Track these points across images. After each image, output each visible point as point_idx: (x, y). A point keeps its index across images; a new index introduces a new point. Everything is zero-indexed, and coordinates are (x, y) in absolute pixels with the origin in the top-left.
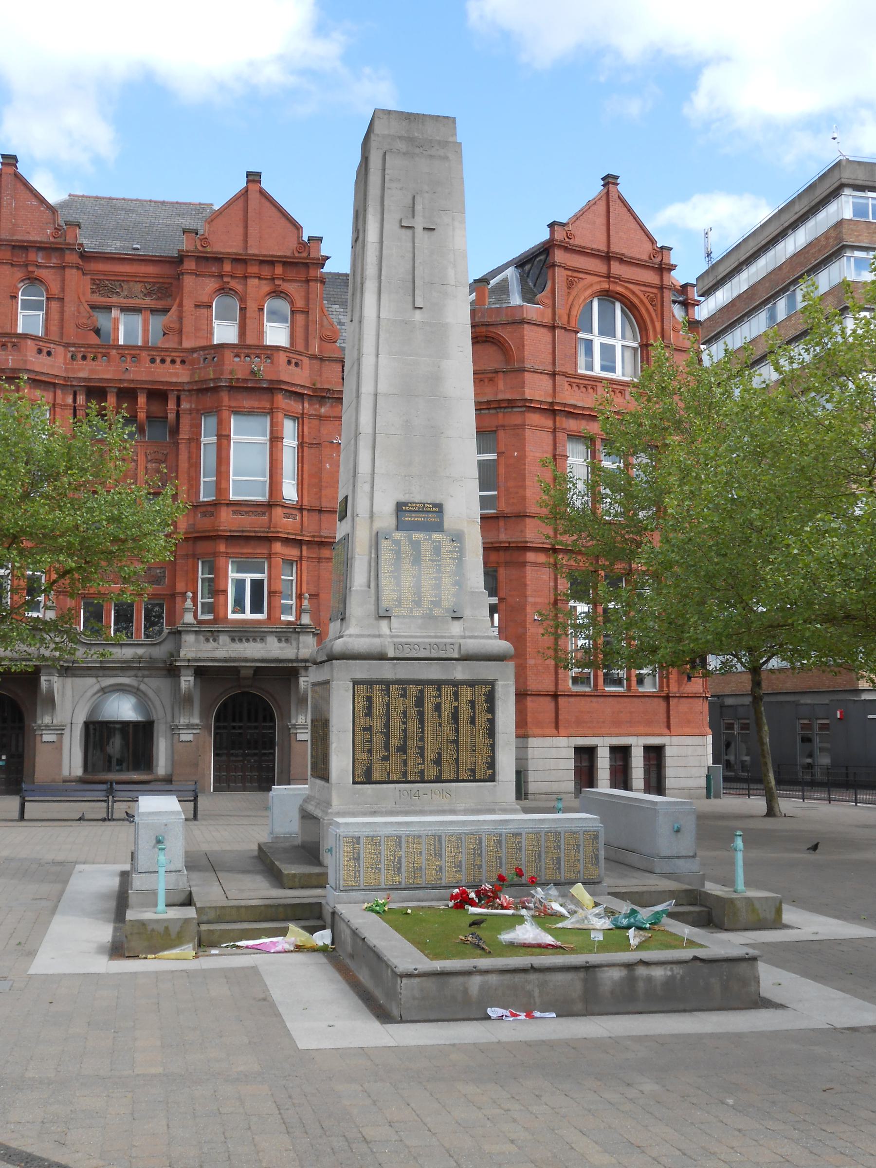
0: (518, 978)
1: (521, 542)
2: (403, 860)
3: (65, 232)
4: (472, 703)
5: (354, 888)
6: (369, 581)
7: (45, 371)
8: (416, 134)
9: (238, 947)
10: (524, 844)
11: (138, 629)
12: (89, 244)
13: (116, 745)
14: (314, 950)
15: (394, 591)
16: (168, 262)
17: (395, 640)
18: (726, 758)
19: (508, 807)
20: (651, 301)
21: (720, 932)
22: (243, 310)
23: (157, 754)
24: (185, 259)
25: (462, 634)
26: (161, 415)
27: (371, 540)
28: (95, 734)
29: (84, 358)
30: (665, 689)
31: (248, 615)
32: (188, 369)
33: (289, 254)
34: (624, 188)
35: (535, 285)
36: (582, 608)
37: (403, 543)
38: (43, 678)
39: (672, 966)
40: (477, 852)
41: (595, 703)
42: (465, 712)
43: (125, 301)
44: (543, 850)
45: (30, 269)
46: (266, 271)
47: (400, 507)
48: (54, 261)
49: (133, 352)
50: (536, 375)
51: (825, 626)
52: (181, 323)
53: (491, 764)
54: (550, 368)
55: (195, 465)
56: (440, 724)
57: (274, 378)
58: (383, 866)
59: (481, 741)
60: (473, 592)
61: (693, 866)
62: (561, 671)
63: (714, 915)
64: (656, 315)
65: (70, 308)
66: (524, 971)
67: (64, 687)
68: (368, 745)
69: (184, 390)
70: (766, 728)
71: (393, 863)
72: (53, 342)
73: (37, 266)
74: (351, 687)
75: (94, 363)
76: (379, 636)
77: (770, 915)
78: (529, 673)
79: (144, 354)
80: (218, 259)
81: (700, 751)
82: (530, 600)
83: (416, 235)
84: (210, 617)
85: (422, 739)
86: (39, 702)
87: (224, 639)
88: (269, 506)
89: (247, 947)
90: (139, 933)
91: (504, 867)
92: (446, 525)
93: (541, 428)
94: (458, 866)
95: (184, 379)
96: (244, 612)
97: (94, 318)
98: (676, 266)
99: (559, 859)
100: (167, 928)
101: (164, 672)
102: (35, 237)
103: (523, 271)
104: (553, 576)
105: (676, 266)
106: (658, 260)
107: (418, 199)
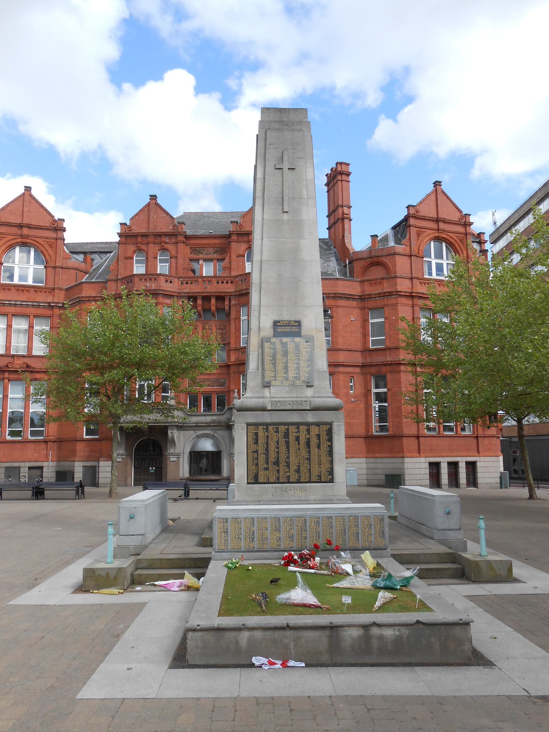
0: (278, 634)
2: (255, 533)
4: (318, 436)
6: (258, 366)
8: (284, 119)
9: (155, 585)
12: (189, 232)
13: (204, 463)
15: (272, 371)
16: (225, 237)
17: (272, 399)
18: (514, 468)
19: (342, 498)
20: (461, 241)
21: (468, 584)
23: (223, 468)
25: (313, 395)
26: (222, 307)
27: (259, 343)
28: (194, 457)
29: (187, 283)
30: (476, 433)
34: (444, 187)
37: (277, 344)
38: (169, 431)
39: (400, 627)
40: (303, 528)
41: (439, 440)
42: (314, 441)
44: (347, 527)
47: (276, 324)
48: (173, 240)
49: (209, 279)
52: (231, 265)
53: (331, 472)
54: (410, 276)
56: (299, 449)
58: (243, 537)
59: (325, 459)
64: (464, 247)
65: (180, 261)
66: (282, 628)
70: (527, 452)
71: (249, 535)
74: (246, 426)
76: (263, 397)
77: (504, 573)
78: (404, 425)
79: (214, 280)
81: (495, 464)
85: (288, 457)
86: (168, 443)
89: (160, 586)
91: (321, 538)
92: (303, 333)
93: (406, 305)
94: (291, 537)
95: (232, 290)
98: (473, 223)
99: (357, 533)
100: (108, 573)
101: (226, 428)
105: (473, 223)
106: (464, 220)
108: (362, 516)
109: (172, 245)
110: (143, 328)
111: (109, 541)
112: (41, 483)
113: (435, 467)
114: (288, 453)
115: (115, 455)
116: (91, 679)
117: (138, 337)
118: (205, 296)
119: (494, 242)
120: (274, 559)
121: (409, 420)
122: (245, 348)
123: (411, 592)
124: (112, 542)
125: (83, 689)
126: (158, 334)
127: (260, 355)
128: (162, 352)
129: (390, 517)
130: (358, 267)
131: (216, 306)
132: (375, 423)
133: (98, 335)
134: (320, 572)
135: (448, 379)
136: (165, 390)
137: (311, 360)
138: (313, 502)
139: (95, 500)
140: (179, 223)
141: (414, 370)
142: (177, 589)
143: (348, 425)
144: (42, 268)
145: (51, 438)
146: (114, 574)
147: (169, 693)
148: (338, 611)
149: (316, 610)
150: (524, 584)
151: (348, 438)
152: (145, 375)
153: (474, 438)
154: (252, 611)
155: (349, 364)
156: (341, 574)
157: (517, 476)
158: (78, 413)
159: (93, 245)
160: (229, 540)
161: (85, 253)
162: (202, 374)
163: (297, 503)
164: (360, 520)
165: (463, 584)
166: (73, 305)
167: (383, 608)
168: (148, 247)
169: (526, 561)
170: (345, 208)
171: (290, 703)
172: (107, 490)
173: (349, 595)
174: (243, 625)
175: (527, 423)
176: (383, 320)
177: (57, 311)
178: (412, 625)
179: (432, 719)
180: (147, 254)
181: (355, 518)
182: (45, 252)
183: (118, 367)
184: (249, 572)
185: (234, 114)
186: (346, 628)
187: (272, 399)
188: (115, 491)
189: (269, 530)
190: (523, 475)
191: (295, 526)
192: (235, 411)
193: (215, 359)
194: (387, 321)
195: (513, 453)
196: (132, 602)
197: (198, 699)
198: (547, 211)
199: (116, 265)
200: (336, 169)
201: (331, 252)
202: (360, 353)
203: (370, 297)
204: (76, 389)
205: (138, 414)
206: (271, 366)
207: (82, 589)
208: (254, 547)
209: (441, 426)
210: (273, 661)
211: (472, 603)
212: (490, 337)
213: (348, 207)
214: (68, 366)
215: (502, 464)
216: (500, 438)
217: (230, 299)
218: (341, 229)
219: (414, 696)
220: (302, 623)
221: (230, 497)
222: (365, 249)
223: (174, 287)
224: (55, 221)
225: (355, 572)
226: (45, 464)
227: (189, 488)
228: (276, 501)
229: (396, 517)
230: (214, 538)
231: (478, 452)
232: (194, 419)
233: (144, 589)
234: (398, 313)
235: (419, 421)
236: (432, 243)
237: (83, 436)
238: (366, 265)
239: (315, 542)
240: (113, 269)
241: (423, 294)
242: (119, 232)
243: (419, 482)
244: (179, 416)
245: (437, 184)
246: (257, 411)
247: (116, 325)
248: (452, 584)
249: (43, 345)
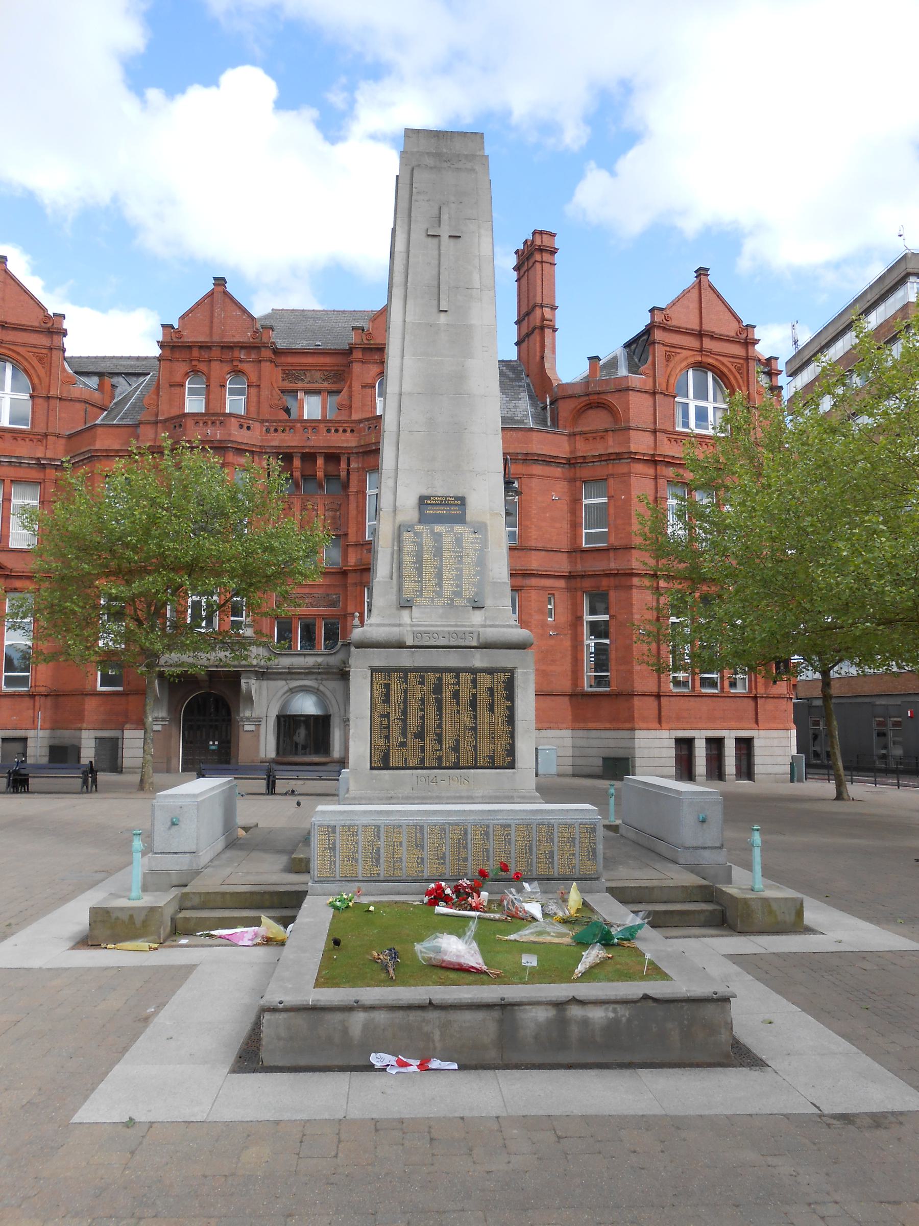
0: (413, 1016)
1: (629, 569)
2: (382, 851)
3: (262, 334)
5: (329, 879)
7: (245, 442)
8: (445, 150)
9: (211, 936)
12: (281, 344)
13: (301, 735)
15: (415, 582)
17: (414, 629)
18: (815, 749)
19: (527, 794)
20: (739, 370)
21: (732, 936)
23: (333, 741)
24: (354, 351)
25: (483, 623)
26: (336, 473)
28: (285, 725)
29: (276, 430)
32: (357, 437)
35: (639, 361)
37: (424, 535)
39: (616, 1006)
40: (461, 844)
41: (693, 702)
42: (483, 699)
43: (308, 385)
44: (534, 843)
45: (235, 363)
47: (423, 501)
48: (253, 356)
53: (511, 751)
54: (651, 426)
56: (458, 712)
58: (360, 857)
59: (501, 728)
60: (495, 582)
63: (728, 914)
64: (743, 381)
65: (265, 393)
66: (421, 1007)
68: (385, 731)
70: (835, 723)
72: (252, 419)
75: (284, 434)
76: (400, 625)
77: (790, 918)
79: (322, 425)
83: (442, 243)
85: (440, 726)
86: (241, 701)
89: (220, 937)
90: (103, 922)
91: (491, 861)
92: (468, 518)
93: (644, 476)
94: (442, 858)
95: (353, 444)
97: (284, 400)
98: (759, 340)
99: (552, 853)
100: (131, 917)
101: (339, 676)
102: (238, 339)
103: (630, 350)
105: (759, 340)
106: (744, 336)
107: (445, 210)
109: (252, 364)
110: (199, 505)
111: (135, 863)
112: (23, 765)
113: (685, 746)
114: (439, 719)
115: (150, 719)
116: (96, 1091)
117: (190, 519)
119: (793, 374)
120: (413, 894)
121: (644, 667)
122: (370, 543)
123: (636, 949)
124: (139, 866)
125: (84, 1107)
126: (226, 516)
127: (395, 553)
128: (232, 548)
129: (608, 827)
130: (566, 409)
131: (325, 471)
132: (588, 674)
133: (121, 515)
134: (487, 915)
135: (711, 601)
136: (236, 612)
137: (481, 563)
138: (480, 800)
139: (114, 795)
140: (263, 327)
141: (655, 585)
142: (250, 943)
143: (542, 674)
144: (26, 398)
145: (42, 690)
146: (142, 917)
147: (228, 1114)
148: (515, 979)
149: (477, 977)
150: (822, 936)
151: (540, 697)
152: (201, 586)
153: (750, 699)
154: (372, 979)
155: (547, 573)
157: (818, 762)
158: (87, 648)
159: (114, 361)
160: (338, 861)
161: (100, 375)
162: (300, 585)
163: (454, 801)
164: (556, 830)
165: (722, 936)
166: (80, 464)
167: (589, 975)
168: (210, 366)
169: (827, 898)
170: (547, 309)
171: (430, 1127)
172: (137, 778)
173: (535, 953)
174: (357, 1002)
175: (837, 676)
176: (605, 500)
177: (52, 474)
179: (662, 1152)
180: (208, 379)
181: (549, 827)
182: (32, 371)
183: (157, 570)
184: (370, 915)
185: (340, 147)
186: (527, 1007)
187: (414, 629)
188: (150, 781)
190: (828, 760)
191: (448, 838)
192: (353, 649)
193: (321, 560)
195: (813, 726)
196: (171, 964)
197: (278, 1122)
198: (882, 324)
199: (155, 397)
200: (533, 241)
201: (520, 384)
202: (565, 555)
203: (584, 460)
204: (83, 608)
205: (189, 650)
207: (87, 941)
209: (697, 678)
210: (405, 1060)
211: (735, 966)
212: (781, 532)
213: (552, 308)
214: (70, 567)
215: (794, 741)
216: (793, 701)
217: (349, 460)
218: (538, 344)
219: (634, 1116)
220: (455, 999)
221: (342, 792)
222: (578, 380)
223: (253, 437)
224: (49, 317)
225: (545, 915)
226: (31, 734)
227: (274, 777)
228: (418, 798)
229: (617, 826)
230: (312, 859)
231: (757, 722)
232: (286, 662)
233: (193, 943)
234: (630, 490)
235: (660, 670)
237: (96, 686)
238: (579, 407)
239: (481, 867)
240: (150, 404)
241: (673, 457)
243: (659, 771)
244: (259, 655)
245: (702, 272)
246: (388, 648)
247: (152, 499)
248: (704, 936)
249: (25, 532)
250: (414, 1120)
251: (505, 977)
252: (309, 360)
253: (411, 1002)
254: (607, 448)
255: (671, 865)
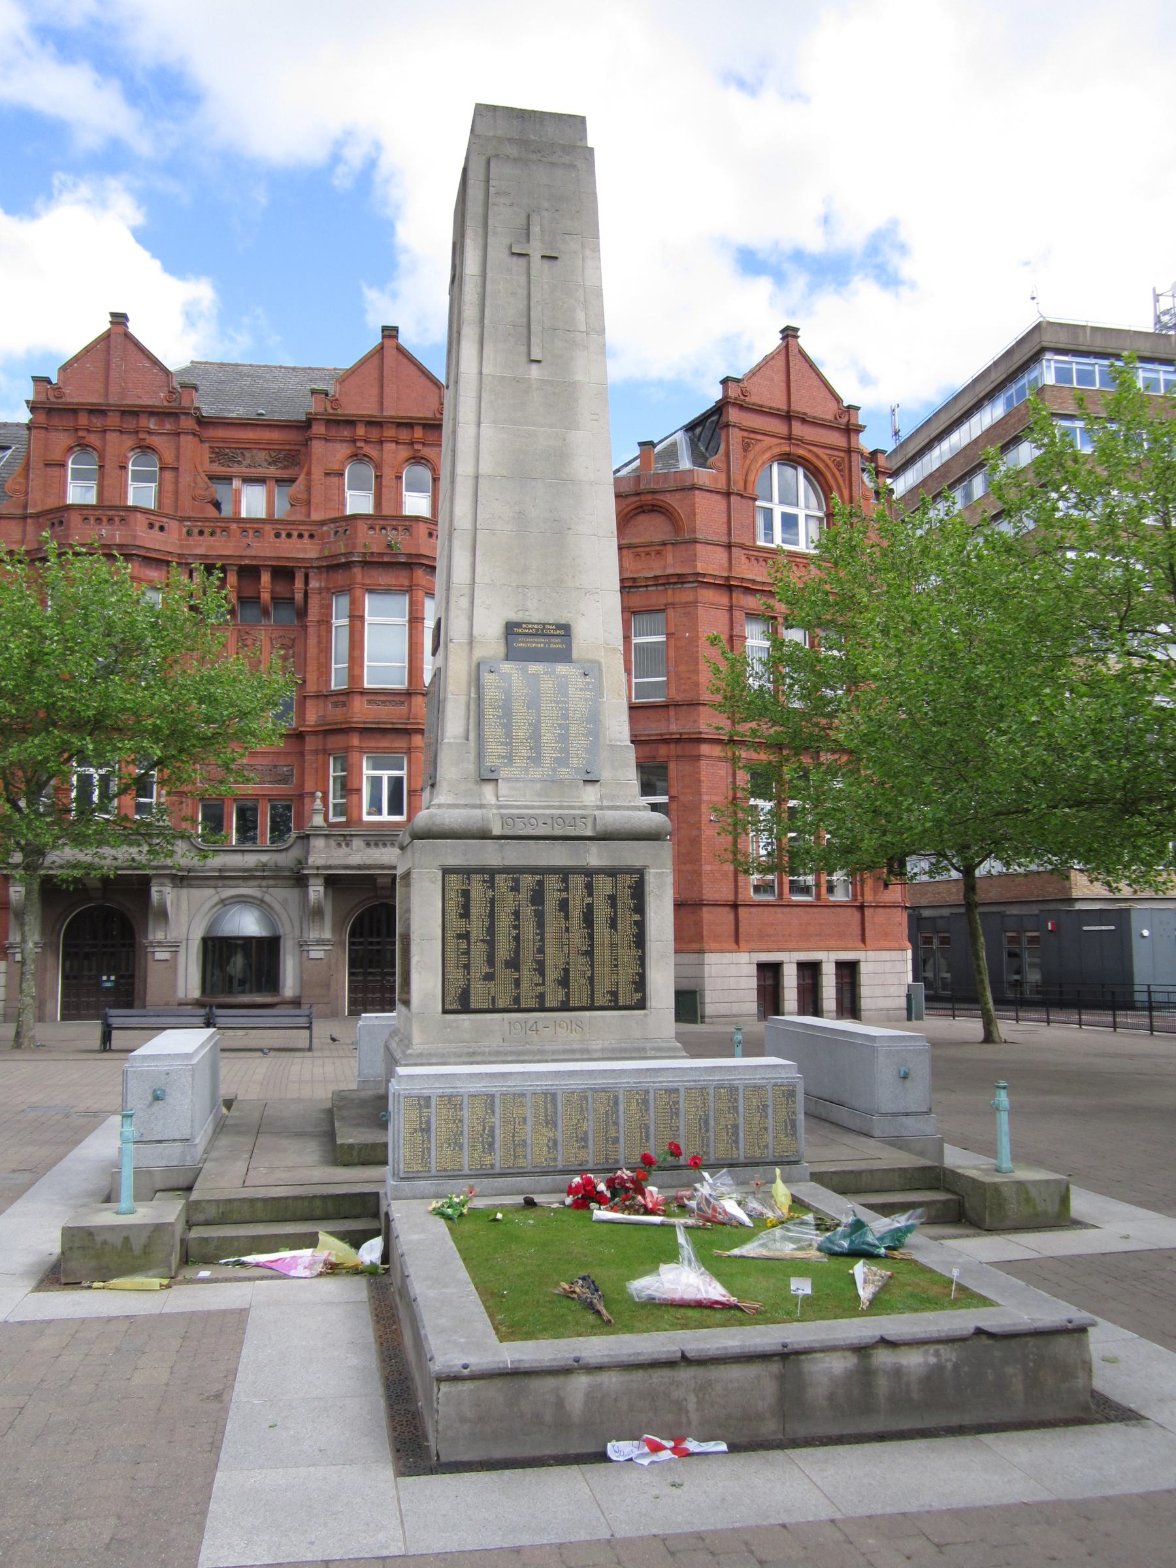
0: (658, 1377)
2: (497, 1132)
4: (613, 899)
6: (467, 731)
8: (532, 137)
9: (243, 1264)
10: (682, 1106)
11: (264, 834)
12: (207, 411)
13: (238, 963)
14: (356, 1271)
15: (502, 744)
17: (503, 811)
19: (665, 1045)
20: (838, 465)
21: (979, 1235)
22: (378, 478)
24: (314, 423)
25: (599, 803)
26: (288, 595)
28: (214, 951)
29: (201, 533)
31: (385, 817)
33: (430, 415)
34: (805, 341)
36: (765, 805)
38: (154, 889)
41: (780, 914)
42: (602, 912)
44: (711, 1113)
45: (141, 436)
46: (404, 435)
47: (511, 629)
48: (168, 426)
49: (255, 526)
50: (709, 547)
51: (1074, 810)
52: (310, 494)
53: (640, 984)
54: (724, 539)
55: (325, 649)
57: (413, 552)
59: (626, 953)
61: (927, 1127)
62: (741, 877)
63: (967, 1205)
65: (186, 479)
66: (670, 1364)
67: (178, 899)
68: (463, 960)
69: (312, 567)
70: (982, 940)
71: (482, 1136)
72: (166, 516)
73: (149, 433)
74: (440, 878)
76: (481, 806)
79: (268, 527)
80: (350, 423)
82: (705, 798)
84: (343, 819)
85: (541, 950)
86: (151, 917)
87: (357, 843)
88: (409, 694)
89: (257, 1265)
91: (652, 1140)
92: (575, 655)
95: (313, 554)
96: (380, 812)
100: (127, 1239)
104: (730, 771)
106: (844, 420)
107: (535, 219)
108: (746, 1086)
113: (770, 973)
118: (246, 565)
127: (472, 703)
131: (272, 592)
137: (594, 719)
138: (599, 1055)
140: (184, 386)
142: (307, 1273)
146: (143, 1240)
156: (724, 1224)
163: (562, 1057)
164: (741, 1095)
165: (968, 1236)
168: (104, 440)
174: (577, 1360)
178: (963, 1339)
180: (102, 457)
187: (503, 811)
188: (31, 1033)
189: (529, 1122)
191: (591, 1111)
194: (672, 642)
199: (22, 480)
206: (500, 732)
208: (492, 1166)
217: (307, 577)
220: (718, 1349)
223: (167, 541)
228: (512, 1053)
231: (863, 941)
234: (696, 624)
236: (775, 467)
240: (15, 491)
241: (754, 582)
242: (31, 398)
245: (789, 333)
250: (715, 1532)
251: (765, 1312)
252: (250, 434)
253: (656, 1356)
254: (665, 568)
255: (864, 1139)
